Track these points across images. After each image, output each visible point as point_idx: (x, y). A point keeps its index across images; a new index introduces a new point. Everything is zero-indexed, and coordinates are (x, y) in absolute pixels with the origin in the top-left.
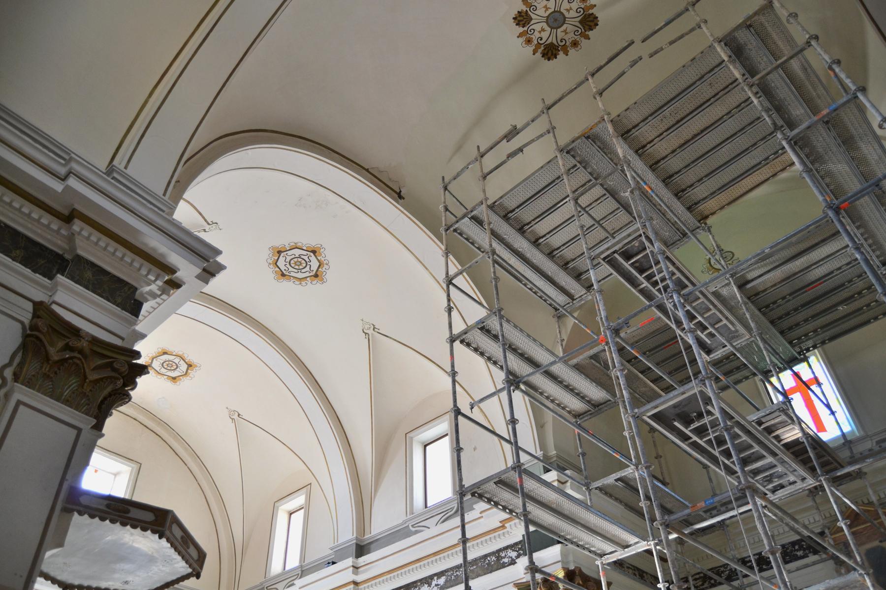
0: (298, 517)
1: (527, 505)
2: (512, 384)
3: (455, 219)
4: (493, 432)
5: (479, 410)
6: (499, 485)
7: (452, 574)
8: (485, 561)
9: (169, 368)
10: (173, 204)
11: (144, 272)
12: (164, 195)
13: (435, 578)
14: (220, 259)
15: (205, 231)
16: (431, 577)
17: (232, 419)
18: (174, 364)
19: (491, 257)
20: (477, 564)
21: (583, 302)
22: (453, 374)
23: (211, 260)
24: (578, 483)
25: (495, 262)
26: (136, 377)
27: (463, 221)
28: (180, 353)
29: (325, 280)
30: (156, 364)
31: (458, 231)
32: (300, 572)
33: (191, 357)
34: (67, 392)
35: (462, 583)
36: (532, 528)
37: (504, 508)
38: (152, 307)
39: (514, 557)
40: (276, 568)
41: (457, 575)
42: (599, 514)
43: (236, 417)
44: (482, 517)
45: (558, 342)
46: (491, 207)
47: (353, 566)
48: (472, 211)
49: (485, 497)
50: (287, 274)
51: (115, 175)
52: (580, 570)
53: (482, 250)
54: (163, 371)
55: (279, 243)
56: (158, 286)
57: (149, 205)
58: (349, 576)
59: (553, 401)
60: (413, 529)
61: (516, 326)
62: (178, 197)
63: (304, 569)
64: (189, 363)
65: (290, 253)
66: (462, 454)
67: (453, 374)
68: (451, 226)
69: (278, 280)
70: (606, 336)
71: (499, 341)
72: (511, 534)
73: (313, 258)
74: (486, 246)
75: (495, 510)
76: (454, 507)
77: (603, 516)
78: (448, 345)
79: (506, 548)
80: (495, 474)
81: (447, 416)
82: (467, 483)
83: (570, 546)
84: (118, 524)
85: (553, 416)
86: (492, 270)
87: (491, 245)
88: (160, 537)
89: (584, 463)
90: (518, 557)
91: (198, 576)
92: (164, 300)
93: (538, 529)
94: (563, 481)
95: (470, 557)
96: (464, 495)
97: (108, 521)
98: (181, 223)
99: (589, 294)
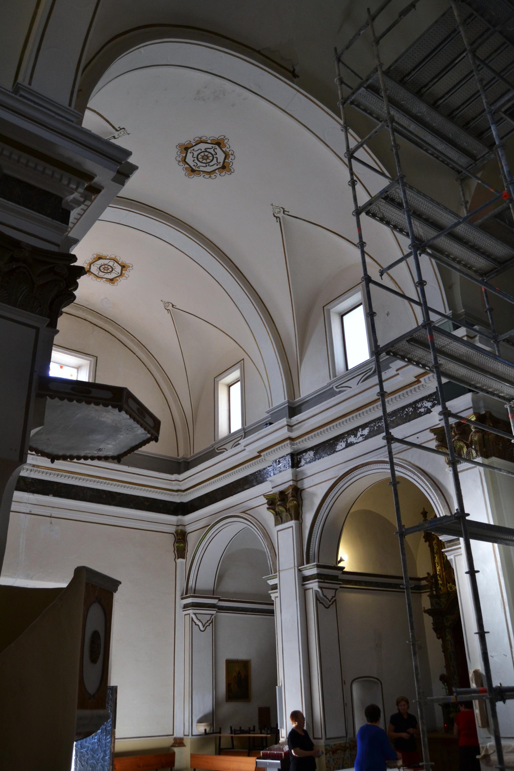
0: (236, 389)
1: (439, 359)
2: (418, 249)
3: (350, 91)
4: (403, 296)
5: (389, 278)
6: (411, 343)
7: (375, 425)
8: (403, 412)
9: (106, 271)
10: (80, 114)
11: (65, 182)
12: (70, 105)
13: (360, 429)
14: (131, 160)
15: (114, 137)
16: (356, 429)
17: (168, 310)
18: (109, 267)
19: (390, 126)
20: (396, 415)
21: (485, 162)
22: (362, 245)
23: (123, 162)
24: (487, 336)
25: (394, 130)
26: (76, 279)
27: (360, 91)
28: (113, 256)
29: (232, 170)
30: (94, 269)
31: (355, 103)
32: (243, 434)
33: (124, 259)
34: (21, 297)
35: (384, 432)
36: (444, 380)
37: (418, 364)
38: (78, 214)
39: (429, 407)
40: (223, 431)
41: (379, 425)
42: (507, 362)
43: (170, 307)
44: (398, 374)
45: (462, 205)
46: (387, 73)
47: (288, 425)
48: (367, 80)
49: (399, 355)
50: (197, 169)
51: (22, 93)
52: (490, 414)
53: (381, 120)
54: (101, 274)
55: (184, 140)
56: (80, 193)
57: (57, 117)
58: (284, 433)
59: (459, 262)
60: (337, 390)
61: (419, 192)
62: (82, 107)
63: (246, 431)
64: (122, 265)
65: (196, 148)
66: (375, 318)
67: (362, 245)
68: (348, 98)
69: (189, 176)
70: (509, 191)
71: (403, 208)
72: (426, 387)
73: (218, 150)
74: (383, 113)
75: (411, 366)
76: (372, 368)
77: (511, 364)
78: (354, 218)
79: (422, 400)
80: (408, 333)
81: (360, 287)
82: (382, 343)
83: (481, 393)
84: (84, 403)
85: (461, 276)
86: (392, 138)
87: (389, 113)
88: (120, 411)
89: (492, 318)
90: (433, 406)
91: (157, 440)
92: (89, 206)
93: (451, 381)
94: (472, 336)
95: (390, 409)
96: (380, 354)
97: (75, 402)
98: (91, 131)
99: (491, 152)
